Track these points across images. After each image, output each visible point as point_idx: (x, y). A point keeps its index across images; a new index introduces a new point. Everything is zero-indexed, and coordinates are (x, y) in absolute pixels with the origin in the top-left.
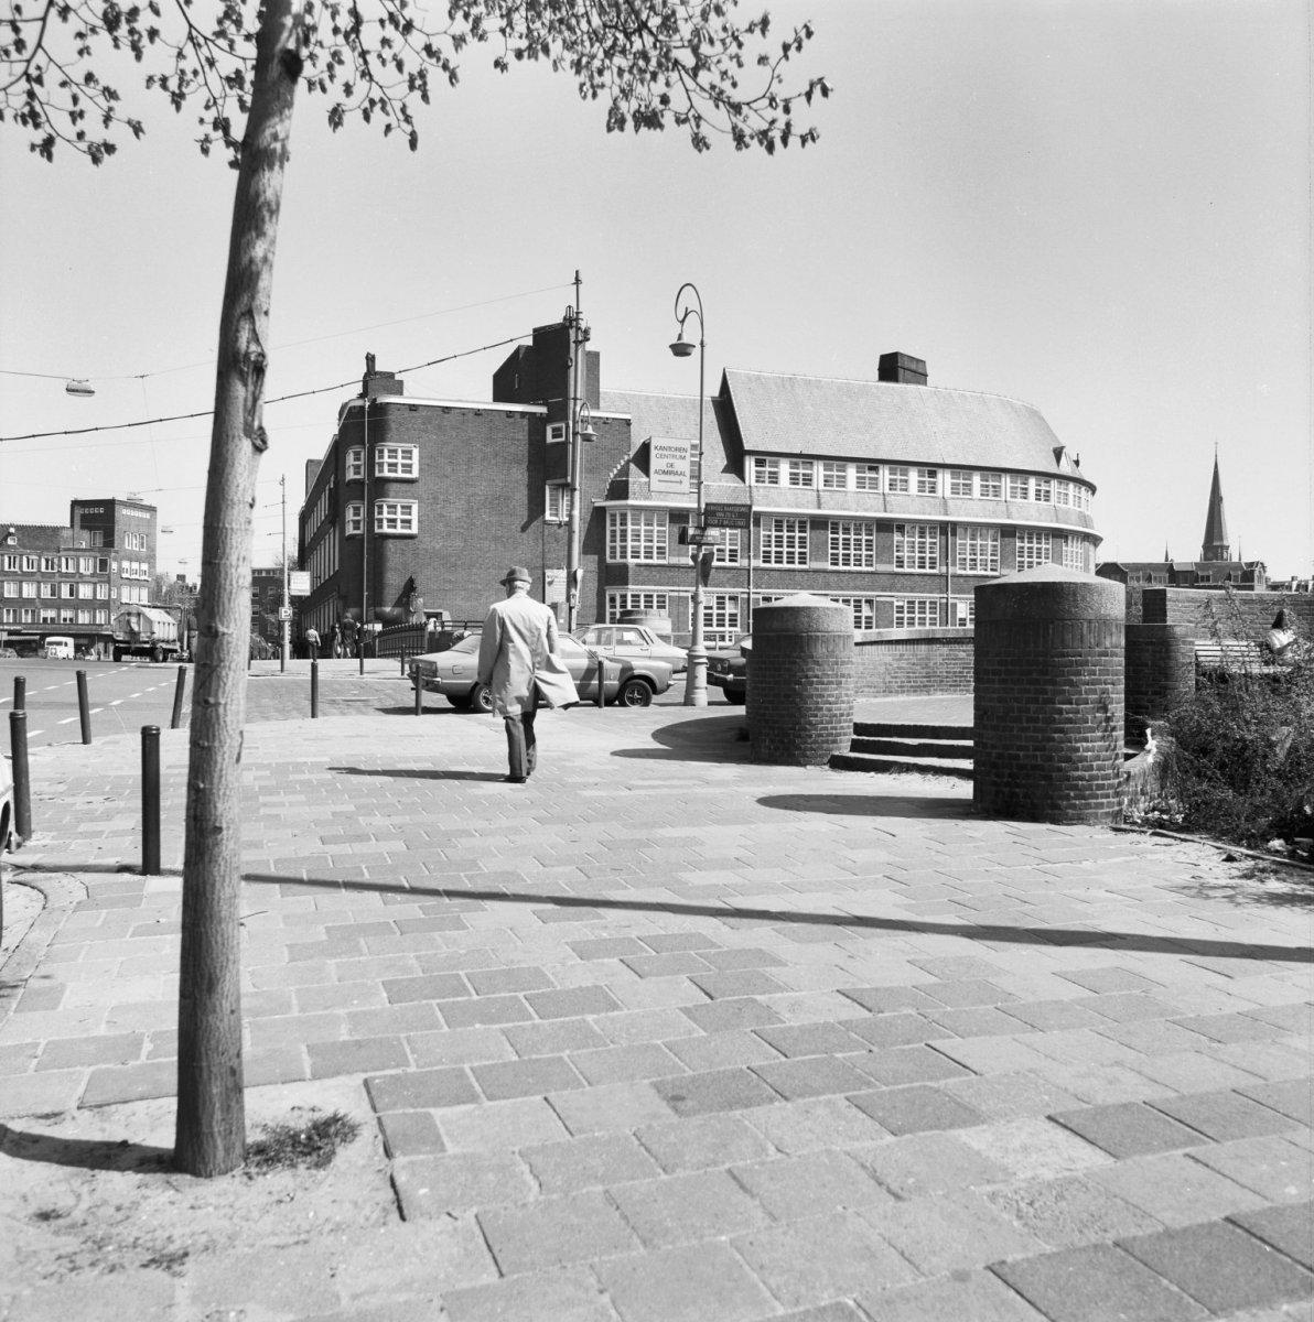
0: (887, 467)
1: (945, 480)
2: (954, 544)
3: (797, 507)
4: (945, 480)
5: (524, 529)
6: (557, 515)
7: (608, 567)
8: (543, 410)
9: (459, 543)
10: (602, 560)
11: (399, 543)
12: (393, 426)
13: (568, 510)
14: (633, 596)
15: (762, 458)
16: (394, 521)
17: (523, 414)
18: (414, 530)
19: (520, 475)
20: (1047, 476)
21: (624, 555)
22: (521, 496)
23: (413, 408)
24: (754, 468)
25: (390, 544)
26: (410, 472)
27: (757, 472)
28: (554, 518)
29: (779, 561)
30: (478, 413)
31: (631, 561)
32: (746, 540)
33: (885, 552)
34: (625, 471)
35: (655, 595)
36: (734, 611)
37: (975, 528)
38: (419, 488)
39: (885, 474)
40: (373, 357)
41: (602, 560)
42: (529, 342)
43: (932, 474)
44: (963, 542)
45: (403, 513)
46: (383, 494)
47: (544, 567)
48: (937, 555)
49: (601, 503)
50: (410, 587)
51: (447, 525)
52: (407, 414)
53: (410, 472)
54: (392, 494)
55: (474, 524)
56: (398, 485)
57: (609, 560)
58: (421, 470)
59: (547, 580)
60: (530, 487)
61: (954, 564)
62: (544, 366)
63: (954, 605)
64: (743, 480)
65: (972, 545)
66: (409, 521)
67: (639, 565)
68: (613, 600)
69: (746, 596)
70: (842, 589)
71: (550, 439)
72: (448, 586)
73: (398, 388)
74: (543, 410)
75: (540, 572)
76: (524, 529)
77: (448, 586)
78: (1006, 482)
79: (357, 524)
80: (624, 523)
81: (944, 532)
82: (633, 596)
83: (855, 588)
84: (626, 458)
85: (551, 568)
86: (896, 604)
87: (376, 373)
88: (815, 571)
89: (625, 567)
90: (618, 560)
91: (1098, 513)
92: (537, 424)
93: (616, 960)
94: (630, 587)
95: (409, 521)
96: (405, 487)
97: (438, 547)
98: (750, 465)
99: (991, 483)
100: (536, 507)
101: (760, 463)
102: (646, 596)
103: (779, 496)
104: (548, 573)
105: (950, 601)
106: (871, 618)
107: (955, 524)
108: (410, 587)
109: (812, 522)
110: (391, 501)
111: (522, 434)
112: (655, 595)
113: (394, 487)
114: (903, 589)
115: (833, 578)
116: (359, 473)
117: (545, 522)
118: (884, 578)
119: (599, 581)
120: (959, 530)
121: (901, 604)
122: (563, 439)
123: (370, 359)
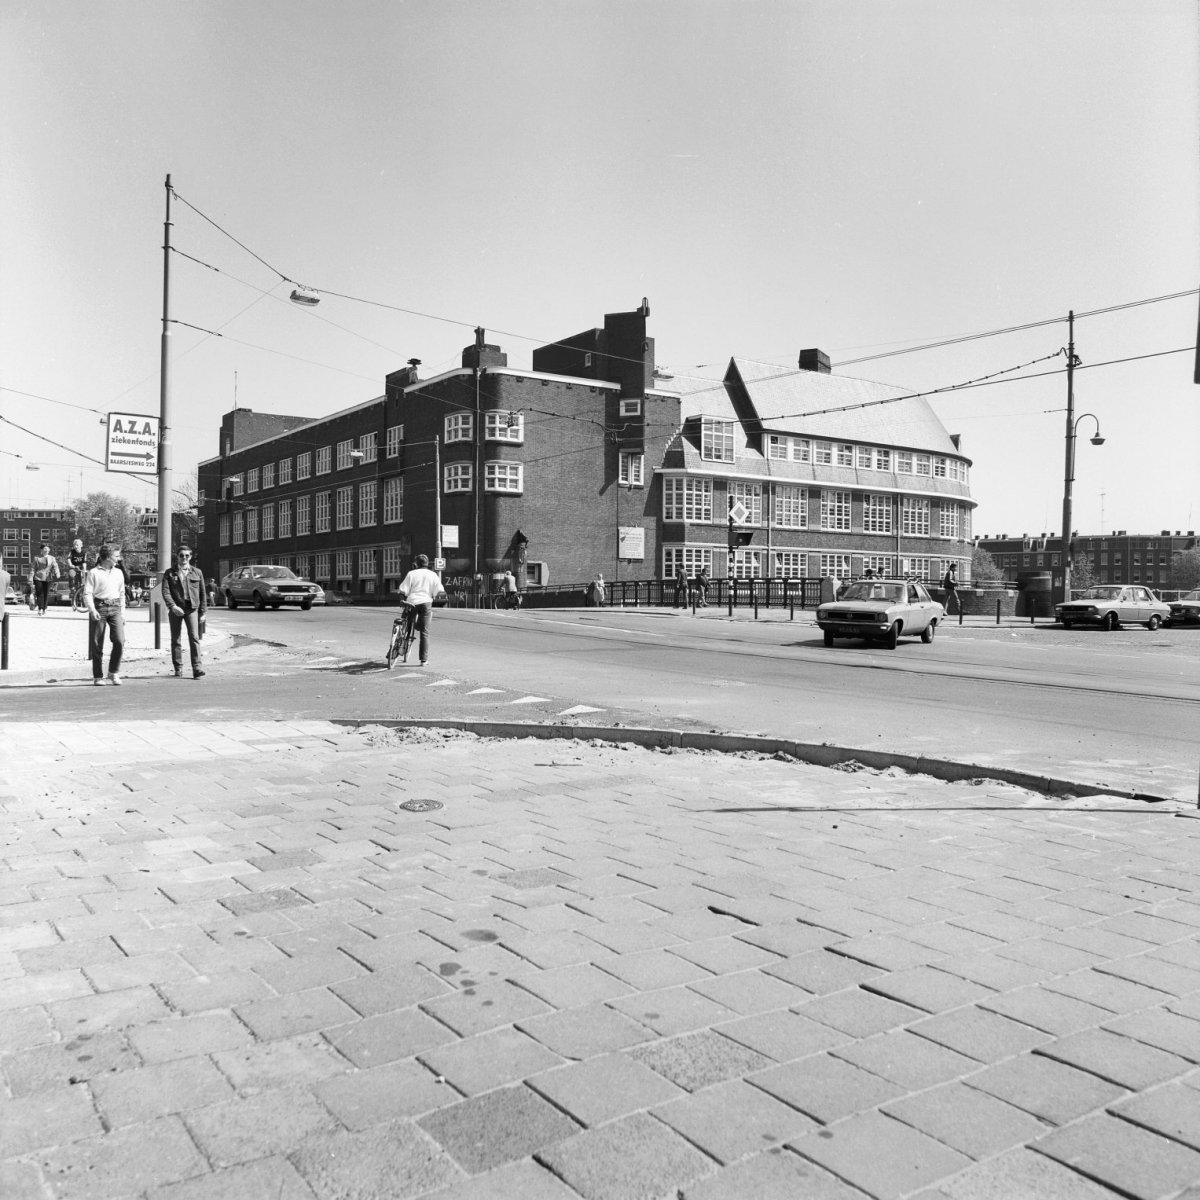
0: (897, 452)
1: (895, 458)
2: (774, 500)
3: (800, 478)
4: (895, 458)
5: (602, 492)
6: (626, 479)
7: (664, 525)
8: (616, 386)
9: (554, 502)
10: (659, 520)
11: (510, 501)
12: (504, 394)
13: (637, 474)
14: (687, 551)
15: (777, 436)
16: (504, 480)
17: (602, 390)
18: (520, 489)
19: (599, 440)
20: (942, 456)
21: (680, 514)
22: (600, 461)
23: (663, 399)
24: (770, 445)
25: (502, 501)
26: (517, 437)
27: (795, 450)
28: (624, 482)
29: (874, 530)
30: (520, 379)
31: (687, 521)
32: (766, 506)
33: (935, 522)
34: (678, 443)
35: (703, 550)
36: (757, 565)
37: (917, 499)
38: (524, 452)
39: (856, 453)
40: (483, 330)
41: (659, 520)
42: (601, 325)
43: (887, 454)
44: (780, 499)
45: (511, 474)
46: (495, 456)
47: (618, 525)
48: (890, 520)
49: (659, 470)
50: (519, 539)
51: (545, 486)
52: (514, 383)
53: (517, 437)
54: (503, 456)
55: (566, 485)
56: (508, 448)
57: (665, 520)
58: (525, 435)
59: (621, 536)
60: (606, 454)
61: (773, 519)
62: (617, 349)
63: (902, 561)
64: (762, 454)
65: (880, 510)
66: (516, 481)
67: (692, 525)
68: (669, 554)
69: (895, 558)
70: (830, 547)
71: (623, 412)
72: (547, 541)
73: (502, 360)
74: (616, 386)
75: (615, 529)
76: (602, 492)
77: (547, 541)
78: (814, 448)
79: (465, 483)
80: (679, 487)
81: (895, 503)
82: (687, 551)
83: (839, 547)
84: (677, 431)
85: (622, 525)
86: (865, 560)
87: (486, 346)
88: (813, 532)
89: (682, 526)
90: (674, 520)
91: (975, 484)
92: (612, 398)
93: (553, 886)
94: (686, 543)
95: (516, 481)
96: (512, 450)
97: (538, 505)
98: (767, 440)
99: (802, 448)
100: (611, 473)
101: (774, 440)
102: (697, 551)
103: (787, 466)
104: (622, 530)
105: (900, 558)
106: (848, 571)
107: (775, 484)
108: (519, 539)
109: (715, 483)
110: (502, 462)
111: (600, 404)
112: (703, 550)
113: (505, 450)
114: (820, 545)
115: (824, 538)
116: (467, 436)
117: (619, 485)
118: (858, 538)
119: (657, 537)
120: (905, 501)
121: (867, 560)
122: (638, 413)
123: (480, 333)
